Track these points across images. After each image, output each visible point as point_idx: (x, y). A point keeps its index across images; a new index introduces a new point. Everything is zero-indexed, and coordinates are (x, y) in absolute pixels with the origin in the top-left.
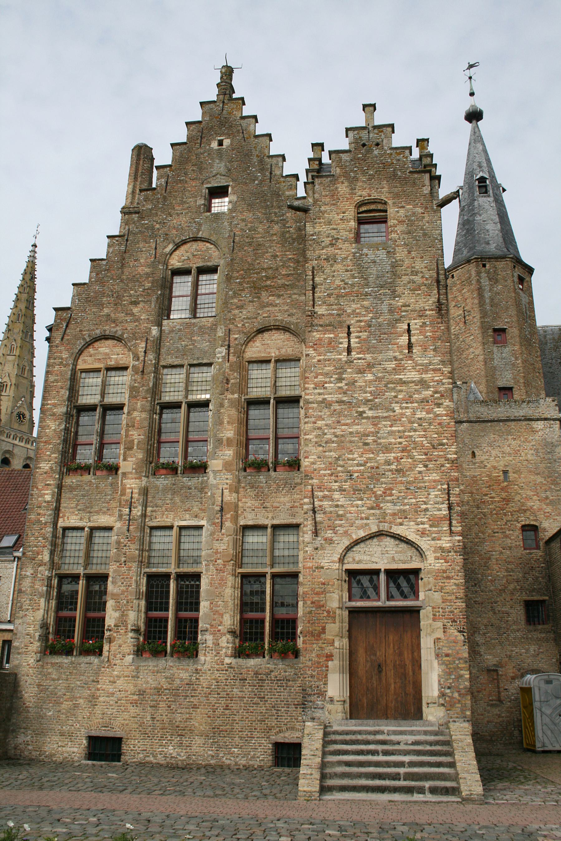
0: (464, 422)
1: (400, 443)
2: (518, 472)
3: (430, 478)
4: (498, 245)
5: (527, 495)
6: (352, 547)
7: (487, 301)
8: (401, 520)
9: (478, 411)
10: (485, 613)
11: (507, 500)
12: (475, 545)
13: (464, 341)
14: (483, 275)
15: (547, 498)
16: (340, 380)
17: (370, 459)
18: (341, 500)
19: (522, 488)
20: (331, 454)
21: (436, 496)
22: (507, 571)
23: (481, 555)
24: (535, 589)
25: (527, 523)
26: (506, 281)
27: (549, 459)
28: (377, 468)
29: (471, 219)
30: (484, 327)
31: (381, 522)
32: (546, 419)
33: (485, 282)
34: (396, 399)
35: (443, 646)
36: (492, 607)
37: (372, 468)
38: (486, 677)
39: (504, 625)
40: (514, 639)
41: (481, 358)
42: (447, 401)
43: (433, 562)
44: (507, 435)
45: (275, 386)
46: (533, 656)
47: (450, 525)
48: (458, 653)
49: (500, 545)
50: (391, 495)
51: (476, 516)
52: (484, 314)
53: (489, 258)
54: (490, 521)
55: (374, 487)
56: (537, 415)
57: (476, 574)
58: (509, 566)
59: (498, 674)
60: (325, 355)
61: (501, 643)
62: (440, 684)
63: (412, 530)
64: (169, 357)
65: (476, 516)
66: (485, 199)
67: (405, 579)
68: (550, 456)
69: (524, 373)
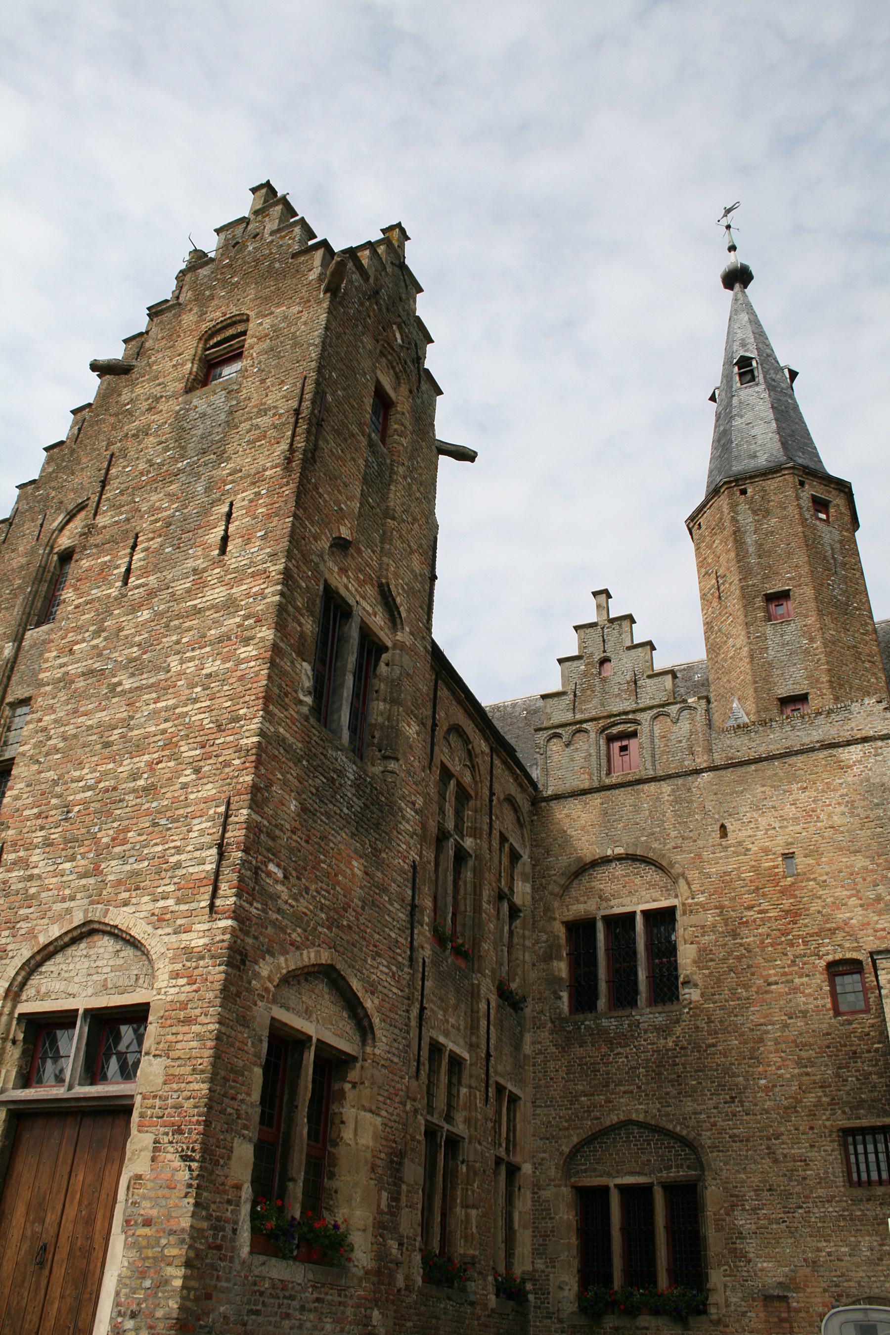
0: (702, 771)
1: (164, 732)
2: (814, 852)
3: (200, 795)
4: (772, 455)
5: (836, 898)
6: (40, 964)
7: (751, 549)
8: (125, 895)
9: (730, 747)
10: (755, 1162)
11: (794, 914)
12: (731, 1013)
13: (720, 630)
14: (743, 507)
15: (879, 899)
16: (97, 634)
17: (105, 773)
18: (41, 864)
19: (823, 885)
20: (48, 774)
21: (202, 833)
22: (799, 1063)
23: (742, 1034)
24: (862, 1101)
25: (838, 956)
26: (785, 508)
27: (879, 818)
28: (115, 789)
29: (728, 427)
30: (747, 597)
31: (92, 903)
32: (865, 740)
33: (746, 518)
34: (178, 647)
35: (144, 1197)
36: (768, 1148)
37: (107, 791)
38: (761, 1315)
39: (798, 1189)
40: (822, 1219)
41: (745, 651)
42: (264, 628)
43: (165, 984)
44: (790, 783)
45: (557, 797)
46: (870, 1262)
47: (214, 895)
48: (169, 1217)
49: (781, 1008)
50: (125, 842)
51: (730, 953)
52: (746, 572)
53: (751, 477)
54: (759, 960)
55: (100, 831)
56: (847, 735)
57: (734, 1075)
58: (803, 1053)
59: (789, 1309)
60: (89, 595)
61: (792, 1232)
62: (117, 1304)
63: (142, 915)
64: (20, 687)
65: (730, 953)
66: (750, 391)
67: (113, 1029)
68: (880, 812)
69: (827, 663)
